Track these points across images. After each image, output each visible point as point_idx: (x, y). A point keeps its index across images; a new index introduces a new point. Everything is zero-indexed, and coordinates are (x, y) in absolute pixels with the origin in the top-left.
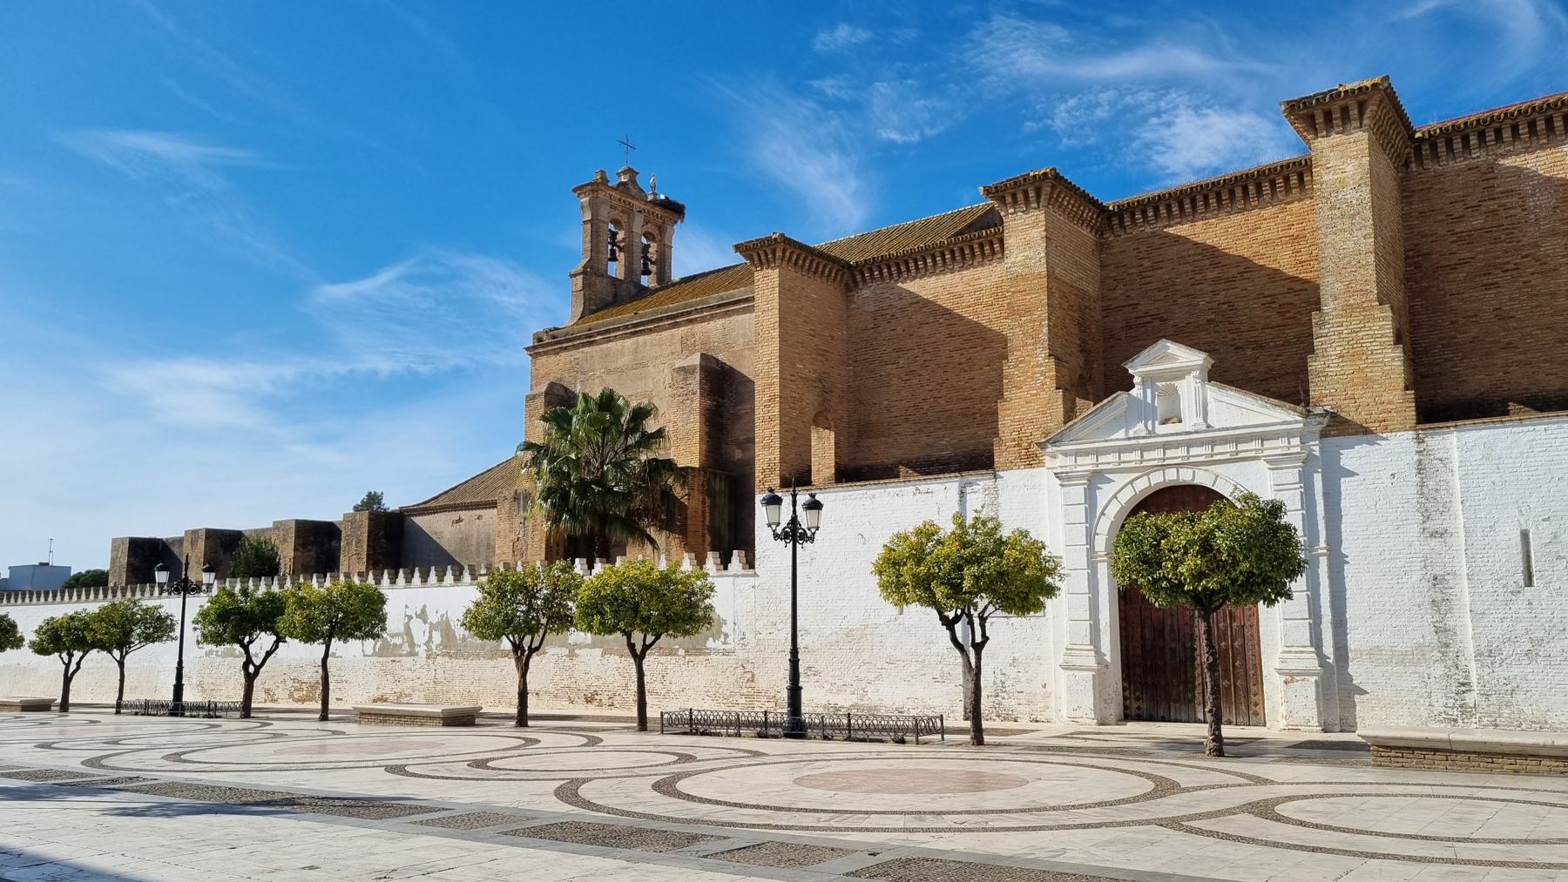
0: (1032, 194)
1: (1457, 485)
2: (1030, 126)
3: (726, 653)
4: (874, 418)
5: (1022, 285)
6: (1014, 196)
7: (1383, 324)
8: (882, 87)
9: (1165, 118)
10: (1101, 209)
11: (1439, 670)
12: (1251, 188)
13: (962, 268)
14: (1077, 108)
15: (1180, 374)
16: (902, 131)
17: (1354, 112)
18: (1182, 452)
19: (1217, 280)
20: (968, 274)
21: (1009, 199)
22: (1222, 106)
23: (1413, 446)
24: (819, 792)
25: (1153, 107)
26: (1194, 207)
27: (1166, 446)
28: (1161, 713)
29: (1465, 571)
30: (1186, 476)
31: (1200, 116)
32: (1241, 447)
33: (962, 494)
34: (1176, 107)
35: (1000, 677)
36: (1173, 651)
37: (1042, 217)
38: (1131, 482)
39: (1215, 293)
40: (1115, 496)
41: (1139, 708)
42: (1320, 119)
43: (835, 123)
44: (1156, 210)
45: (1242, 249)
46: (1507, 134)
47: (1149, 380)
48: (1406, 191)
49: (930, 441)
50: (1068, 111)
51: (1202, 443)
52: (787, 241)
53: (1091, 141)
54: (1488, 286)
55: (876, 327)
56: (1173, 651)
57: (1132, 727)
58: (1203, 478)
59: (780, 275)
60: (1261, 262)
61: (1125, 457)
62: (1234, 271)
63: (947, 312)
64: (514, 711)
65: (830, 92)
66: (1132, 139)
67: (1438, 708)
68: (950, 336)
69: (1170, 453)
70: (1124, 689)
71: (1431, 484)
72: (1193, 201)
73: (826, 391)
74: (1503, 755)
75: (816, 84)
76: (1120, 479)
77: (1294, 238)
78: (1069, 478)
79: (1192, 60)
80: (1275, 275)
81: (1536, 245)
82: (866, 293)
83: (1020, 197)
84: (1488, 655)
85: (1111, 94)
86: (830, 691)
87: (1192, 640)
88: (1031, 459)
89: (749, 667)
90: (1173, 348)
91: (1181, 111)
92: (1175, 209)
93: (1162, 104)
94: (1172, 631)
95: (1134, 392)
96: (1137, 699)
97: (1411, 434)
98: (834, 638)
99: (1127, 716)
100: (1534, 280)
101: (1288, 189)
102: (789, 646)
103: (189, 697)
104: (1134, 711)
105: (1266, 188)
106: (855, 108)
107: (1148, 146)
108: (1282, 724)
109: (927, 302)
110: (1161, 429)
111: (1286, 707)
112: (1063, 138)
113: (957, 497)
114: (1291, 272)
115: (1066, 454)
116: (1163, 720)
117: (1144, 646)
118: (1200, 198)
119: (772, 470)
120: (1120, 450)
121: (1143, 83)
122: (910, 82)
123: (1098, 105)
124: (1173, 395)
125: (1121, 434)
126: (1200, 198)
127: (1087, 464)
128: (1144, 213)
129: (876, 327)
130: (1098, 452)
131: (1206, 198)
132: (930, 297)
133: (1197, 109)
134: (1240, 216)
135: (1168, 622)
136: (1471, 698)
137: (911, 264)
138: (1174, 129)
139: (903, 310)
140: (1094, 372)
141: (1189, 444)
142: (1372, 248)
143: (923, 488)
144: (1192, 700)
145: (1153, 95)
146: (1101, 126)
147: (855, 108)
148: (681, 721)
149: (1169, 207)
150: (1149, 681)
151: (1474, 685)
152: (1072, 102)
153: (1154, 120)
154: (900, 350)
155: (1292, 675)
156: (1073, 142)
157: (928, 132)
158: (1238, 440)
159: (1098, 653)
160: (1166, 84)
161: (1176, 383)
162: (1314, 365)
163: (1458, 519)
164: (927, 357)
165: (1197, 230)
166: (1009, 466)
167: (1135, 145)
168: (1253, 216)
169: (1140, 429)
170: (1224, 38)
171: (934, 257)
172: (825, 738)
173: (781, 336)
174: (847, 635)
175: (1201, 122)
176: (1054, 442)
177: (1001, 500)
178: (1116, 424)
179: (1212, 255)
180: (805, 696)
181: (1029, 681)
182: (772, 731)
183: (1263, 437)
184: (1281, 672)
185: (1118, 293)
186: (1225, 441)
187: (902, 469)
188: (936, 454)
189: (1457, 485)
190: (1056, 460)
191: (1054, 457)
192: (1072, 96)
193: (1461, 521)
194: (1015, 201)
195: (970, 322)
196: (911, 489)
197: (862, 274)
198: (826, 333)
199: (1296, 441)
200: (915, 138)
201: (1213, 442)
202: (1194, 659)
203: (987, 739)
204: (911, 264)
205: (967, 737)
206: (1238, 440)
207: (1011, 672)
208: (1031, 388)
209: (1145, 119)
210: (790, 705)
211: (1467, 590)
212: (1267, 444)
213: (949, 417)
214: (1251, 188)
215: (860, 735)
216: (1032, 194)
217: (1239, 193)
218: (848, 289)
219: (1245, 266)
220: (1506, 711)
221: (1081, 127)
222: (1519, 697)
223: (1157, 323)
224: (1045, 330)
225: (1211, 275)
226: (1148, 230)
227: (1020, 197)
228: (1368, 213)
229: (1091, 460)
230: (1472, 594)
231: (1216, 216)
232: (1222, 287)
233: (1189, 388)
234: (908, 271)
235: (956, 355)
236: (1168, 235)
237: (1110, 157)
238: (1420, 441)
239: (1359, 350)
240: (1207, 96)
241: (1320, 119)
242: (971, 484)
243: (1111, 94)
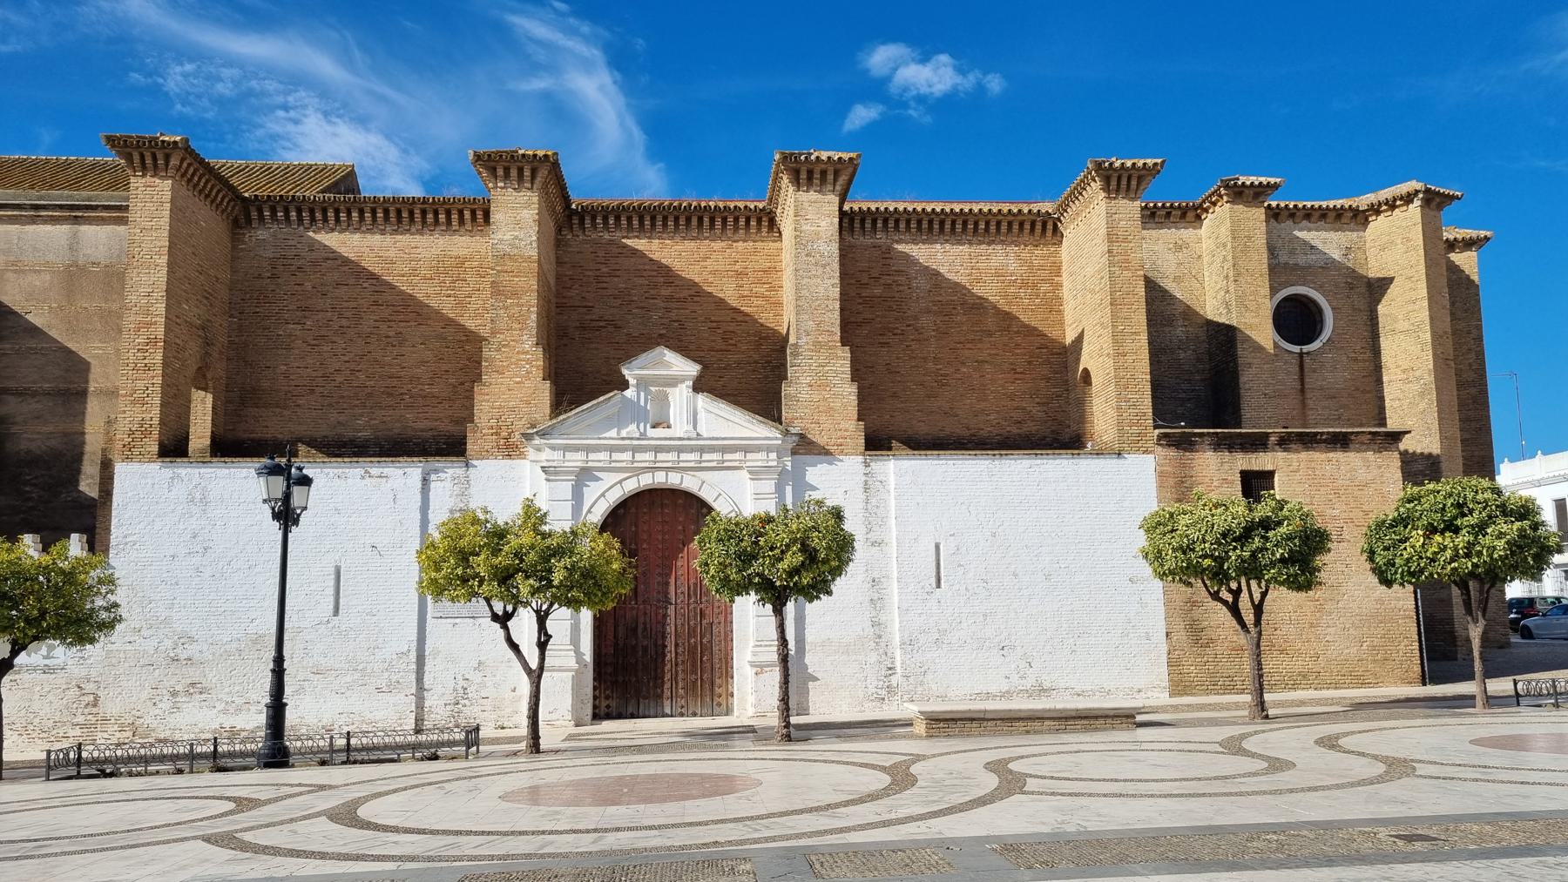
0: (527, 173)
1: (893, 503)
3: (47, 670)
4: (265, 384)
5: (509, 265)
6: (507, 170)
7: (841, 362)
9: (292, 114)
11: (873, 658)
12: (706, 220)
13: (395, 232)
14: (195, 75)
15: (674, 382)
17: (830, 177)
18: (672, 456)
19: (669, 299)
20: (404, 240)
21: (500, 172)
22: (352, 119)
23: (862, 467)
24: (622, 809)
25: (280, 99)
26: (653, 225)
27: (658, 449)
28: (630, 710)
29: (895, 575)
30: (674, 480)
31: (329, 122)
32: (727, 456)
33: (425, 481)
34: (305, 107)
35: (461, 683)
36: (645, 649)
37: (535, 199)
38: (620, 482)
39: (668, 310)
40: (603, 495)
41: (608, 707)
42: (803, 175)
44: (618, 218)
45: (692, 273)
46: (902, 225)
47: (643, 384)
48: (559, 243)
49: (342, 418)
51: (692, 449)
52: (187, 149)
53: (210, 115)
54: (883, 344)
55: (274, 277)
56: (645, 649)
57: (607, 725)
58: (689, 483)
59: (173, 189)
60: (709, 290)
61: (616, 456)
62: (686, 293)
63: (373, 276)
67: (872, 689)
68: (376, 303)
69: (661, 456)
70: (595, 688)
71: (874, 501)
72: (653, 219)
73: (208, 343)
74: (1020, 719)
76: (609, 479)
77: (739, 274)
78: (556, 473)
79: (323, 65)
80: (721, 303)
81: (916, 318)
82: (262, 234)
83: (514, 173)
84: (909, 644)
85: (235, 72)
86: (225, 712)
87: (664, 638)
88: (510, 450)
89: (90, 687)
90: (670, 356)
91: (310, 111)
92: (635, 222)
93: (290, 99)
94: (645, 629)
95: (629, 393)
96: (607, 698)
97: (860, 459)
98: (235, 645)
99: (597, 716)
100: (914, 346)
101: (736, 229)
102: (272, 653)
103: (822, 706)
104: (603, 710)
105: (718, 223)
107: (274, 137)
108: (751, 711)
109: (346, 261)
110: (651, 432)
111: (752, 693)
112: (179, 101)
113: (419, 485)
114: (734, 303)
115: (553, 448)
116: (633, 716)
117: (616, 644)
118: (660, 218)
119: (146, 433)
120: (612, 449)
121: (269, 70)
123: (220, 79)
124: (663, 401)
125: (613, 433)
126: (660, 218)
127: (576, 460)
128: (605, 219)
129: (274, 277)
130: (589, 449)
131: (665, 219)
132: (352, 256)
133: (326, 114)
134: (693, 244)
135: (641, 620)
136: (894, 680)
137: (331, 214)
138: (300, 128)
139: (315, 263)
140: (581, 373)
141: (680, 450)
142: (837, 296)
143: (375, 471)
144: (660, 696)
145: (281, 87)
146: (220, 102)
148: (67, 763)
149: (629, 219)
150: (620, 679)
151: (899, 670)
152: (189, 67)
153: (281, 113)
154: (307, 309)
155: (762, 667)
156: (187, 110)
158: (724, 450)
159: (579, 655)
160: (296, 80)
161: (668, 390)
162: (786, 390)
163: (892, 532)
164: (344, 322)
165: (654, 248)
166: (484, 455)
167: (260, 133)
168: (705, 246)
169: (632, 429)
170: (357, 54)
171: (361, 212)
173: (170, 265)
174: (255, 642)
175: (329, 128)
176: (543, 434)
177: (473, 490)
178: (610, 422)
179: (665, 272)
180: (291, 717)
181: (496, 685)
182: (85, 770)
183: (747, 450)
184: (753, 664)
185: (573, 293)
186: (712, 449)
187: (302, 448)
188: (349, 434)
189: (893, 503)
190: (540, 454)
191: (539, 450)
192: (191, 60)
193: (894, 535)
194: (507, 176)
195: (403, 292)
196: (359, 471)
197: (260, 211)
198: (212, 272)
199: (773, 456)
201: (702, 450)
202: (664, 656)
204: (331, 214)
205: (523, 746)
206: (724, 450)
207: (476, 677)
208: (515, 376)
209: (273, 108)
211: (896, 591)
212: (749, 456)
213: (370, 395)
214: (706, 220)
215: (364, 756)
216: (527, 173)
217: (694, 221)
218: (236, 224)
219: (695, 292)
220: (920, 689)
221: (199, 96)
222: (929, 676)
223: (611, 329)
224: (534, 317)
225: (665, 292)
226: (607, 236)
227: (514, 173)
228: (836, 266)
229: (580, 456)
230: (900, 594)
231: (672, 238)
232: (674, 305)
233: (681, 398)
234: (325, 220)
235: (383, 326)
236: (625, 246)
237: (229, 137)
238: (867, 465)
239: (823, 384)
240: (336, 106)
241: (803, 175)
242: (436, 471)
243: (235, 72)
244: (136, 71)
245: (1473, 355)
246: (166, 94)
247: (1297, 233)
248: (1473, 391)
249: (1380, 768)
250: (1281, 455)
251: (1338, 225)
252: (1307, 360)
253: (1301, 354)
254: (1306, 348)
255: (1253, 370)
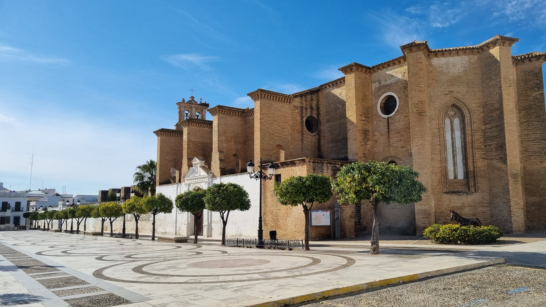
2: (496, 14)
8: (433, 7)
10: (369, 68)
14: (516, 5)
16: (442, 23)
43: (415, 23)
50: (512, 6)
52: (262, 91)
53: (522, 17)
64: (221, 238)
65: (413, 12)
66: (541, 14)
71: (437, 164)
75: (407, 9)
76: (192, 185)
106: (423, 17)
122: (446, 4)
147: (423, 17)
156: (515, 18)
157: (453, 22)
172: (291, 249)
200: (447, 25)
203: (310, 248)
205: (221, 242)
210: (259, 236)
244: (495, 12)
245: (498, 96)
246: (506, 16)
247: (388, 72)
248: (498, 112)
249: (103, 258)
250: (282, 169)
251: (400, 65)
252: (390, 120)
253: (388, 118)
254: (390, 116)
255: (351, 132)
